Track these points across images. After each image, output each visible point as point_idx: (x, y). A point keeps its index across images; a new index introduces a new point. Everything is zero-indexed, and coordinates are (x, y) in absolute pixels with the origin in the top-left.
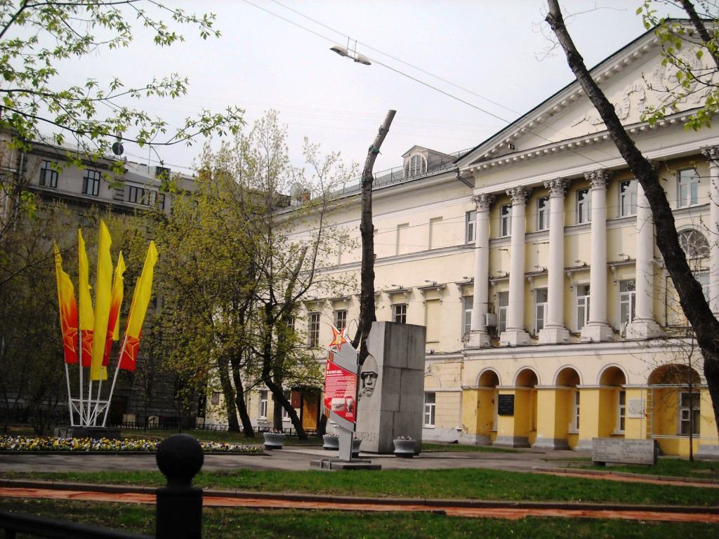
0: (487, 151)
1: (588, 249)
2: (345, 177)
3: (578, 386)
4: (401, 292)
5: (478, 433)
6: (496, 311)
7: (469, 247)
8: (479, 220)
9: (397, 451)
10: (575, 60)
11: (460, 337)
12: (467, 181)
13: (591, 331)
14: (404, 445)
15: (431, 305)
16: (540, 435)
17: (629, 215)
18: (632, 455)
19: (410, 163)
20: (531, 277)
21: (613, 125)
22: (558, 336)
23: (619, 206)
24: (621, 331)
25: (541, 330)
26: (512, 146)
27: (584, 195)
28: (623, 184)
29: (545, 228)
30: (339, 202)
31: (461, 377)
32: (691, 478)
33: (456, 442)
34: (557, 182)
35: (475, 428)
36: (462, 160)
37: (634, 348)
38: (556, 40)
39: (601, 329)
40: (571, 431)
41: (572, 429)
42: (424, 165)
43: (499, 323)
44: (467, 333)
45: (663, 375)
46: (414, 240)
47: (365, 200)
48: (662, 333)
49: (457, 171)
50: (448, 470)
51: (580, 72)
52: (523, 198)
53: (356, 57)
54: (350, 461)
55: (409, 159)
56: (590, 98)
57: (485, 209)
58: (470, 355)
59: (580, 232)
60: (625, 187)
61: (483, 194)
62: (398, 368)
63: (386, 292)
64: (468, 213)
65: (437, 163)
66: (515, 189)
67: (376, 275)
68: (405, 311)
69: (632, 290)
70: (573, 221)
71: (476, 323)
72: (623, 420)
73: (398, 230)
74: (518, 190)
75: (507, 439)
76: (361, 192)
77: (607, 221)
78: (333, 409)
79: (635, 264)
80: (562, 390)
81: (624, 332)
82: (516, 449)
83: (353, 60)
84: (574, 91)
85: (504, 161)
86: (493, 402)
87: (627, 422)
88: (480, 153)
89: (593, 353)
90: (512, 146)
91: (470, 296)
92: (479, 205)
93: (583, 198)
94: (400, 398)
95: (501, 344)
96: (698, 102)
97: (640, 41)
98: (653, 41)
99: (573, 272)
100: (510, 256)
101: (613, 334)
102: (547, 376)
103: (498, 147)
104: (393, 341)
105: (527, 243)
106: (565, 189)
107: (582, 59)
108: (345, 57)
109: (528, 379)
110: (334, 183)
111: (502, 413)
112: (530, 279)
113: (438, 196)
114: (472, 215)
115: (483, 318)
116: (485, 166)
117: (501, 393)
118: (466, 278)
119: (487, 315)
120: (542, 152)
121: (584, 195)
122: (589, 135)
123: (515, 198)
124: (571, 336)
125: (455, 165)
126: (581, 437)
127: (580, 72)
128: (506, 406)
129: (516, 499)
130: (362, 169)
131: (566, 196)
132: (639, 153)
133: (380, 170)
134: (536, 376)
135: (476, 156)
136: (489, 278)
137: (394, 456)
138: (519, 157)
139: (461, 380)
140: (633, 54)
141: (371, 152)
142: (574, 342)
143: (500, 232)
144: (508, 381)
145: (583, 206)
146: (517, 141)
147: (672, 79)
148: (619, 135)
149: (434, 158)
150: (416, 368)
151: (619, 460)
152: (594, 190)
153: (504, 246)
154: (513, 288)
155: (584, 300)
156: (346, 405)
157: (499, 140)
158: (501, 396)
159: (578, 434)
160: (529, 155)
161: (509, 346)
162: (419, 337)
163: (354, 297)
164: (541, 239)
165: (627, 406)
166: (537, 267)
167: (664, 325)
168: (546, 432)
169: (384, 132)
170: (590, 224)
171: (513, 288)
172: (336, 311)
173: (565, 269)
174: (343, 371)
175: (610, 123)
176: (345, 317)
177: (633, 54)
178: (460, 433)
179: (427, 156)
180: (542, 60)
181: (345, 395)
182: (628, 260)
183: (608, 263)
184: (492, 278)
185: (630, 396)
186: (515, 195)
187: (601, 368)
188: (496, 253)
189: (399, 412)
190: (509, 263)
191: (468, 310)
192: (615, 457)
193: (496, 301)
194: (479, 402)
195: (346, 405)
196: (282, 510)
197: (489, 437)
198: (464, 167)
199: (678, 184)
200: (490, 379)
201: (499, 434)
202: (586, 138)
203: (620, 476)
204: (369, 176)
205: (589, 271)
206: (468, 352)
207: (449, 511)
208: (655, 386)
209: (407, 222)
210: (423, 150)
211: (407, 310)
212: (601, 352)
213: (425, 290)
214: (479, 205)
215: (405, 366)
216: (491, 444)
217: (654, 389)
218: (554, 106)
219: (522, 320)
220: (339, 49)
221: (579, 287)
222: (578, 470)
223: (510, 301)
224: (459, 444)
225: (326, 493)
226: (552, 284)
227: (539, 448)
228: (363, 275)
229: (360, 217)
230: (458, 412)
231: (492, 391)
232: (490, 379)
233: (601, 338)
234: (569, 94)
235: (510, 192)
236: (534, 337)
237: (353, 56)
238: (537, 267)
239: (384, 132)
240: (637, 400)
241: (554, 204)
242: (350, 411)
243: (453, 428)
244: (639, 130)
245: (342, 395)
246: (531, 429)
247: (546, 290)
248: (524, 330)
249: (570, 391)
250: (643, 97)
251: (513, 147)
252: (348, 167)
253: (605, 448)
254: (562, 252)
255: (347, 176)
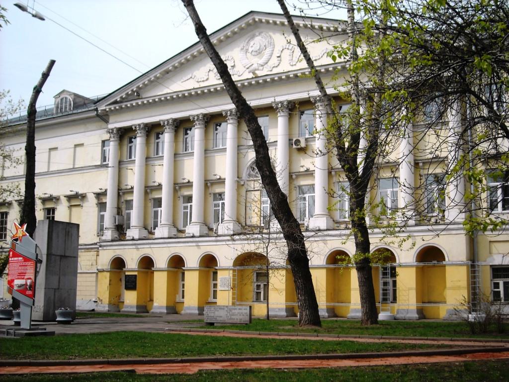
0: (119, 97)
1: (191, 170)
2: (12, 110)
3: (183, 268)
4: (51, 199)
5: (110, 304)
6: (123, 213)
7: (103, 166)
8: (112, 148)
9: (58, 319)
10: (200, 29)
11: (96, 233)
12: (104, 118)
13: (193, 229)
14: (63, 314)
15: (74, 209)
16: (155, 304)
17: (221, 147)
18: (233, 317)
19: (60, 102)
20: (150, 189)
21: (227, 79)
22: (169, 232)
23: (214, 139)
24: (214, 229)
25: (156, 228)
26: (138, 94)
27: (188, 132)
28: (217, 125)
29: (160, 154)
30: (8, 129)
31: (96, 262)
32: (283, 333)
33: (93, 310)
34: (170, 121)
35: (108, 300)
36: (101, 102)
37: (228, 240)
38: (188, 15)
39: (200, 227)
40: (177, 300)
41: (179, 298)
42: (70, 105)
43: (125, 222)
44: (101, 229)
45: (245, 260)
46: (61, 160)
47: (29, 127)
48: (244, 229)
49: (96, 110)
50: (101, 334)
51: (204, 38)
52: (145, 132)
53: (34, 13)
54: (30, 330)
55: (59, 100)
56: (211, 58)
57: (116, 139)
58: (105, 246)
59: (185, 158)
60: (218, 127)
61: (115, 128)
62: (58, 256)
63: (16, 201)
64: (103, 142)
65: (80, 103)
66: (139, 125)
67: (36, 185)
68: (54, 213)
69: (190, 203)
70: (181, 150)
71: (108, 222)
72: (215, 292)
73: (49, 152)
74: (142, 126)
75: (132, 307)
76: (26, 122)
77: (146, 158)
78: (16, 288)
79: (192, 185)
80: (171, 271)
81: (217, 230)
82: (137, 314)
83: (31, 15)
84: (185, 57)
85: (132, 104)
86: (121, 280)
87: (219, 294)
88: (113, 98)
89: (194, 244)
90: (138, 94)
91: (103, 203)
92: (112, 136)
93: (188, 134)
94: (59, 278)
95: (127, 238)
96: (271, 71)
97: (233, 25)
98: (241, 25)
99: (124, 192)
100: (134, 174)
101: (209, 231)
102: (161, 260)
103: (127, 94)
104: (54, 235)
105: (147, 165)
106: (176, 127)
107: (206, 30)
108: (25, 13)
109: (147, 263)
110: (4, 114)
111: (128, 288)
112: (148, 191)
113: (81, 128)
114: (106, 143)
115: (113, 218)
116: (117, 108)
117: (127, 273)
118: (101, 189)
119: (117, 216)
120: (160, 99)
121: (188, 132)
122: (194, 89)
123: (139, 132)
124: (178, 233)
125: (94, 105)
126: (186, 305)
127: (204, 38)
128: (131, 283)
129: (176, 356)
130: (27, 103)
131: (290, 117)
132: (245, 100)
133: (40, 106)
134: (152, 260)
135: (110, 100)
136: (119, 190)
137: (56, 323)
138: (143, 102)
139: (96, 265)
140: (227, 34)
141: (35, 91)
142: (181, 236)
143: (127, 157)
144: (132, 264)
145: (188, 140)
146: (142, 90)
147: (253, 53)
148: (232, 89)
149: (78, 100)
150: (72, 256)
151: (225, 321)
152: (230, 123)
153: (130, 166)
154: (136, 198)
155: (187, 207)
156: (26, 284)
157: (128, 89)
158: (126, 276)
159: (184, 302)
160: (151, 101)
161: (133, 239)
162: (74, 231)
163: (14, 202)
164: (157, 163)
165: (219, 282)
166: (154, 182)
167: (244, 225)
168: (160, 300)
169: (45, 76)
170: (135, 160)
171: (136, 198)
172: (46, 208)
173: (175, 184)
174: (23, 258)
175: (225, 77)
176: (6, 217)
177: (227, 34)
178: (96, 304)
179: (73, 98)
180: (178, 27)
181: (26, 277)
182: (220, 179)
183: (205, 181)
184: (121, 190)
185: (220, 275)
186: (139, 130)
187: (138, 257)
188: (123, 171)
189: (58, 289)
190: (133, 178)
191: (102, 213)
192: (221, 319)
193: (123, 206)
194: (110, 281)
195: (26, 284)
196: (17, 376)
197: (118, 306)
198: (102, 107)
199: (299, 121)
200: (118, 263)
201: (125, 303)
202: (192, 91)
203: (230, 332)
204: (33, 109)
205: (192, 186)
206: (103, 244)
207: (141, 369)
208: (238, 268)
209: (56, 147)
210: (70, 93)
211: (56, 212)
212: (200, 244)
213: (70, 198)
214: (112, 136)
215: (63, 255)
216: (119, 311)
217: (238, 270)
218: (169, 67)
219: (142, 221)
220: (21, 5)
221: (184, 197)
222: (200, 329)
223: (107, 207)
224: (96, 312)
225: (25, 358)
226: (165, 195)
227: (156, 313)
228: (26, 184)
229: (26, 140)
230: (94, 288)
231: (120, 272)
232: (118, 263)
233: (327, 227)
234: (181, 59)
235: (135, 127)
236: (151, 233)
237: (31, 12)
238: (154, 182)
239: (45, 76)
240: (225, 278)
241: (167, 137)
242: (30, 290)
243: (90, 300)
244: (327, 71)
245: (23, 277)
246: (149, 299)
247: (161, 199)
248: (144, 227)
249: (177, 271)
250: (233, 65)
251: (138, 95)
252: (15, 102)
253: (214, 313)
254: (144, 174)
255: (14, 109)
